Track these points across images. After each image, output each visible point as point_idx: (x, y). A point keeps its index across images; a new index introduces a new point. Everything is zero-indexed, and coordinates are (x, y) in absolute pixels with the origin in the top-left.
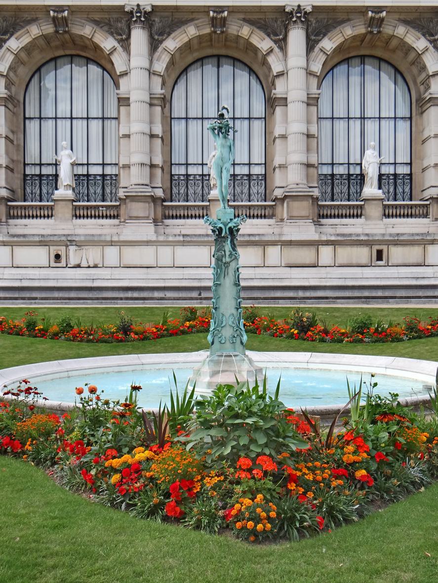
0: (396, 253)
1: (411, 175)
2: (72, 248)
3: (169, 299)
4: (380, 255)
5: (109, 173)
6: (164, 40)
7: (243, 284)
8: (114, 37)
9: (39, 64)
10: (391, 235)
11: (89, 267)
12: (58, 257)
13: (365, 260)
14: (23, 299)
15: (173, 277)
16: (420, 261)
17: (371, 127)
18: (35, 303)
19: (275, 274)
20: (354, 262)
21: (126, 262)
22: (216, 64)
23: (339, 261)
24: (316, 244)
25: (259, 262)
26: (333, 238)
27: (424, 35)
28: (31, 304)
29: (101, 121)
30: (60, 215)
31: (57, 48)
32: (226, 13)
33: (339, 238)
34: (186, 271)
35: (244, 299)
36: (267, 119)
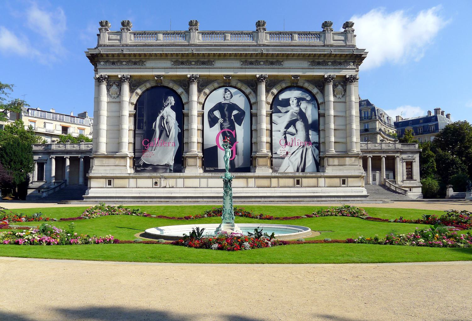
0: (116, 182)
4: (298, 182)
6: (136, 89)
7: (233, 195)
8: (182, 87)
11: (170, 187)
12: (156, 183)
13: (291, 184)
20: (287, 185)
21: (186, 185)
23: (281, 185)
24: (270, 178)
27: (316, 87)
28: (145, 204)
32: (299, 78)
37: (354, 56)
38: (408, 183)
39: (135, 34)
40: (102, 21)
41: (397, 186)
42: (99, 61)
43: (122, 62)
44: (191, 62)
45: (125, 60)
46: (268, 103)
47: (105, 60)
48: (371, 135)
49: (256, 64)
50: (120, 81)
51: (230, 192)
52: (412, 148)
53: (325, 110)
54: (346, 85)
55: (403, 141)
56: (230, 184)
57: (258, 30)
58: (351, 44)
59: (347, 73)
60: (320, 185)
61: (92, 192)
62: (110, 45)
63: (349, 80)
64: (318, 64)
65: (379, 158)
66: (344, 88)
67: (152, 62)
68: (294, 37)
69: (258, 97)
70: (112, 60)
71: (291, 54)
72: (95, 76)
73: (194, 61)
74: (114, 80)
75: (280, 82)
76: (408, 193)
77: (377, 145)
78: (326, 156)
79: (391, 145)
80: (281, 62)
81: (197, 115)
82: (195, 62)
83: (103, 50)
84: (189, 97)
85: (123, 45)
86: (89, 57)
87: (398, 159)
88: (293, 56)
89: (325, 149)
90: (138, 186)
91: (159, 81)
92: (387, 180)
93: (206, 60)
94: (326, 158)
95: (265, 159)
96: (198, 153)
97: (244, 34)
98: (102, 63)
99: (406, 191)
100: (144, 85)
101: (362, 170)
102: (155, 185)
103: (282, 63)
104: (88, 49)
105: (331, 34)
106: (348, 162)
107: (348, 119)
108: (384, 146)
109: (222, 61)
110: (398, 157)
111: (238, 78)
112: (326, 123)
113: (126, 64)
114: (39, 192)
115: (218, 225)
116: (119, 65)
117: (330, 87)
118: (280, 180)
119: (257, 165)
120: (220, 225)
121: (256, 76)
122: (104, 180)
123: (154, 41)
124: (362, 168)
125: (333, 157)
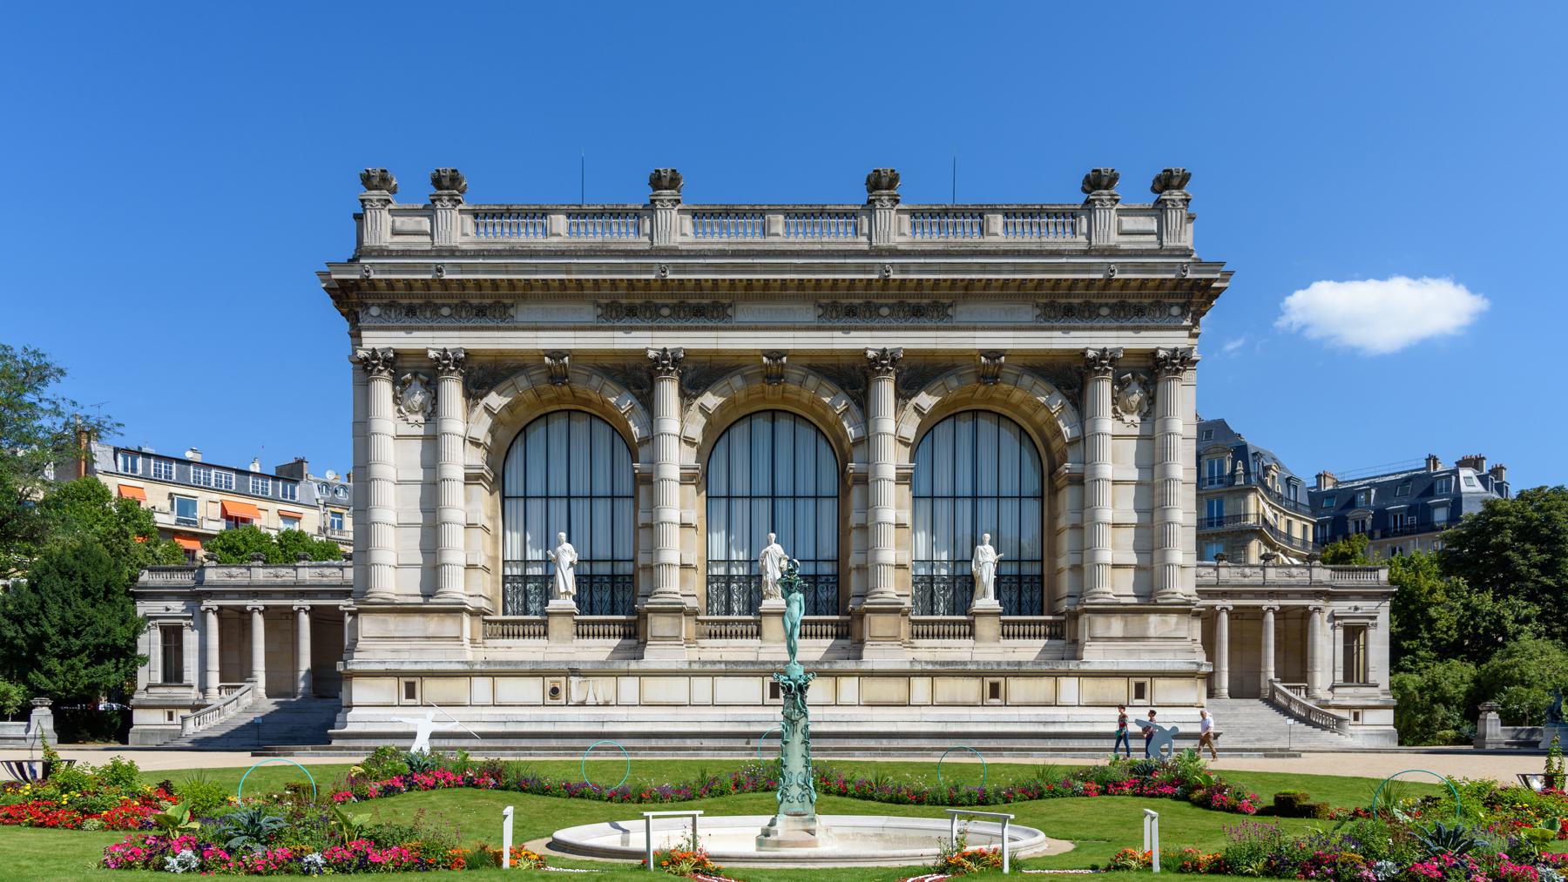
0: (431, 689)
1: (1041, 576)
2: (574, 680)
3: (708, 749)
4: (994, 691)
5: (621, 572)
7: (812, 729)
9: (524, 423)
10: (1009, 663)
11: (598, 705)
14: (512, 749)
15: (710, 720)
16: (1051, 699)
17: (986, 508)
18: (531, 755)
19: (850, 715)
20: (959, 700)
21: (648, 698)
22: (770, 419)
23: (939, 698)
25: (830, 699)
26: (930, 667)
27: (1058, 387)
29: (544, 500)
30: (556, 634)
31: (550, 401)
32: (785, 359)
33: (937, 667)
34: (730, 711)
35: (813, 749)
36: (842, 496)
37: (1186, 284)
38: (1349, 696)
39: (476, 216)
40: (368, 171)
41: (1311, 704)
42: (366, 304)
43: (437, 308)
44: (658, 308)
45: (378, 301)
46: (903, 441)
47: (385, 301)
48: (1231, 538)
49: (868, 315)
50: (436, 368)
51: (802, 722)
52: (1366, 581)
53: (1085, 463)
54: (1155, 383)
55: (1340, 561)
56: (802, 699)
57: (874, 200)
58: (1179, 244)
59: (1164, 341)
60: (1063, 699)
61: (357, 720)
62: (397, 251)
63: (1166, 365)
64: (847, 315)
65: (1258, 615)
66: (1148, 392)
67: (533, 306)
68: (991, 224)
69: (1088, 424)
70: (405, 302)
71: (980, 280)
72: (355, 353)
73: (666, 306)
74: (415, 364)
75: (941, 373)
76: (1350, 728)
77: (1247, 571)
78: (1087, 611)
79: (1294, 571)
80: (945, 307)
81: (893, 477)
82: (673, 308)
83: (377, 267)
84: (652, 422)
85: (441, 250)
86: (333, 289)
87: (1317, 616)
88: (1002, 288)
89: (1083, 586)
90: (500, 699)
91: (559, 370)
92: (1280, 686)
93: (705, 301)
94: (1087, 615)
95: (891, 618)
96: (683, 600)
97: (829, 214)
98: (374, 311)
99: (1340, 720)
100: (508, 383)
101: (1201, 657)
102: (552, 697)
103: (950, 311)
104: (329, 264)
105: (1113, 212)
106: (1155, 627)
107: (1157, 491)
108: (1272, 574)
109: (757, 306)
110: (1320, 609)
111: (806, 361)
112: (1086, 505)
113: (451, 315)
114: (171, 717)
115: (766, 819)
116: (428, 315)
117: (1104, 390)
118: (939, 682)
119: (867, 638)
120: (772, 824)
121: (865, 354)
122: (392, 682)
123: (976, 238)
124: (1198, 646)
125: (1109, 611)
